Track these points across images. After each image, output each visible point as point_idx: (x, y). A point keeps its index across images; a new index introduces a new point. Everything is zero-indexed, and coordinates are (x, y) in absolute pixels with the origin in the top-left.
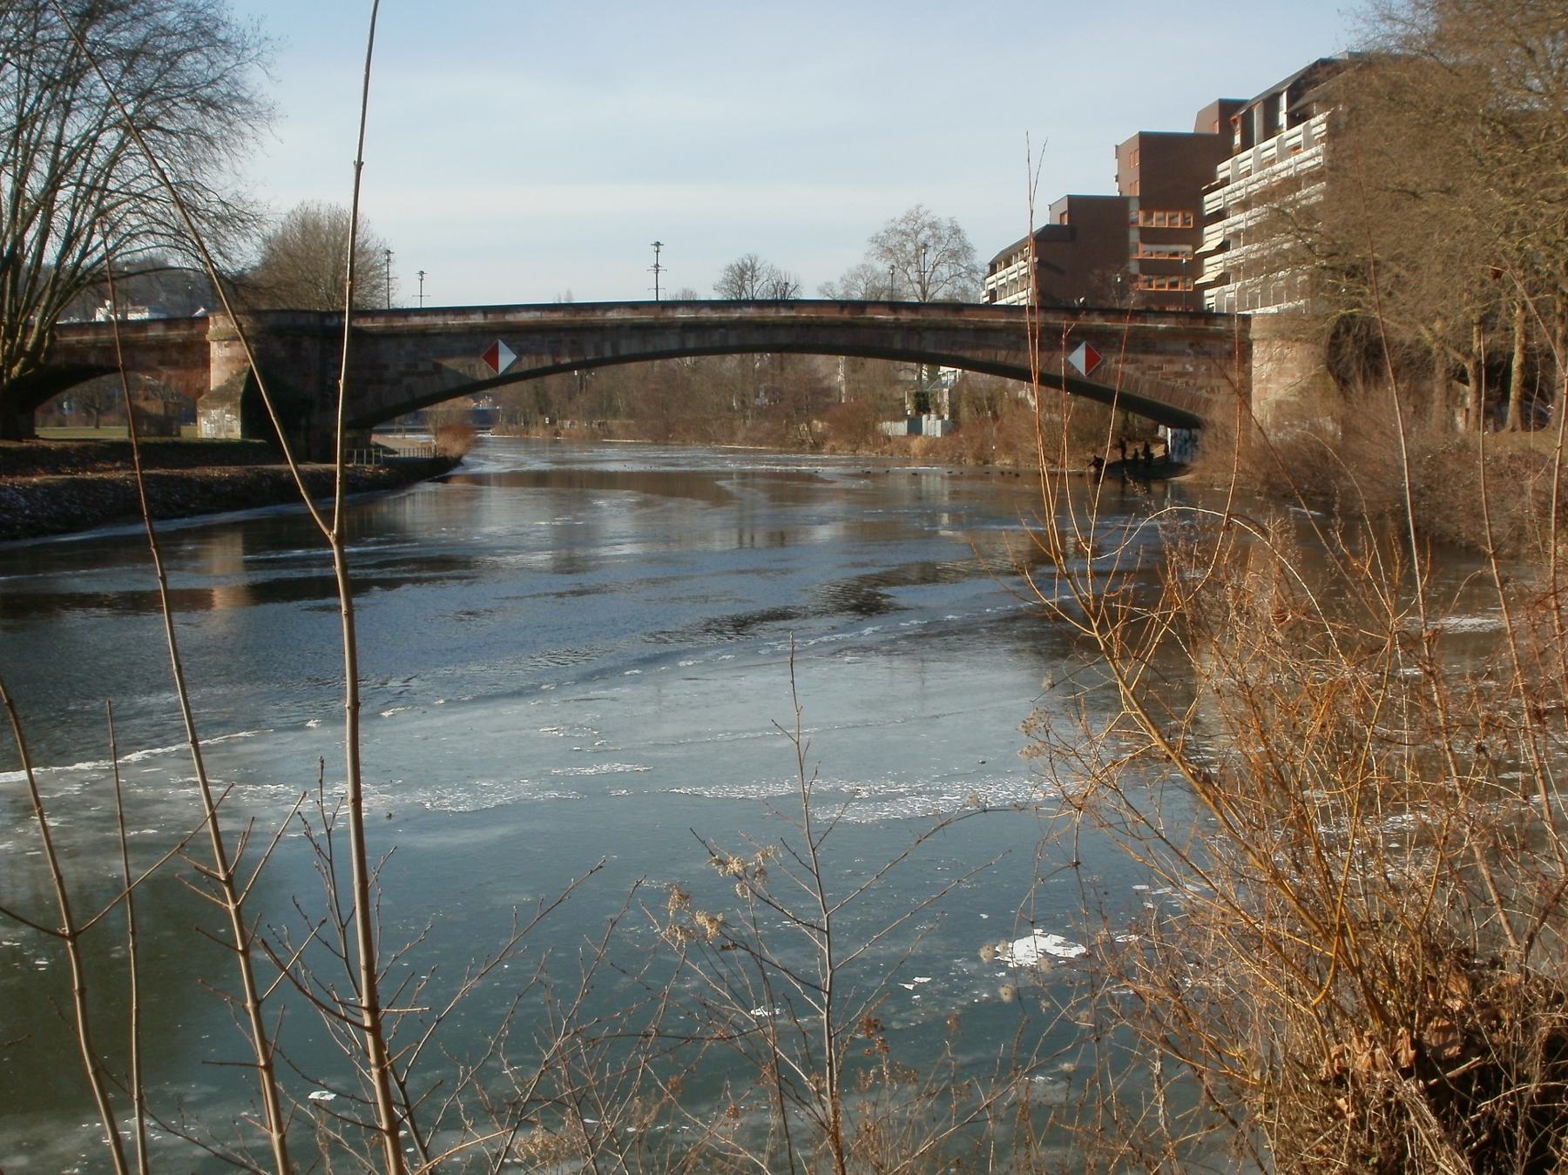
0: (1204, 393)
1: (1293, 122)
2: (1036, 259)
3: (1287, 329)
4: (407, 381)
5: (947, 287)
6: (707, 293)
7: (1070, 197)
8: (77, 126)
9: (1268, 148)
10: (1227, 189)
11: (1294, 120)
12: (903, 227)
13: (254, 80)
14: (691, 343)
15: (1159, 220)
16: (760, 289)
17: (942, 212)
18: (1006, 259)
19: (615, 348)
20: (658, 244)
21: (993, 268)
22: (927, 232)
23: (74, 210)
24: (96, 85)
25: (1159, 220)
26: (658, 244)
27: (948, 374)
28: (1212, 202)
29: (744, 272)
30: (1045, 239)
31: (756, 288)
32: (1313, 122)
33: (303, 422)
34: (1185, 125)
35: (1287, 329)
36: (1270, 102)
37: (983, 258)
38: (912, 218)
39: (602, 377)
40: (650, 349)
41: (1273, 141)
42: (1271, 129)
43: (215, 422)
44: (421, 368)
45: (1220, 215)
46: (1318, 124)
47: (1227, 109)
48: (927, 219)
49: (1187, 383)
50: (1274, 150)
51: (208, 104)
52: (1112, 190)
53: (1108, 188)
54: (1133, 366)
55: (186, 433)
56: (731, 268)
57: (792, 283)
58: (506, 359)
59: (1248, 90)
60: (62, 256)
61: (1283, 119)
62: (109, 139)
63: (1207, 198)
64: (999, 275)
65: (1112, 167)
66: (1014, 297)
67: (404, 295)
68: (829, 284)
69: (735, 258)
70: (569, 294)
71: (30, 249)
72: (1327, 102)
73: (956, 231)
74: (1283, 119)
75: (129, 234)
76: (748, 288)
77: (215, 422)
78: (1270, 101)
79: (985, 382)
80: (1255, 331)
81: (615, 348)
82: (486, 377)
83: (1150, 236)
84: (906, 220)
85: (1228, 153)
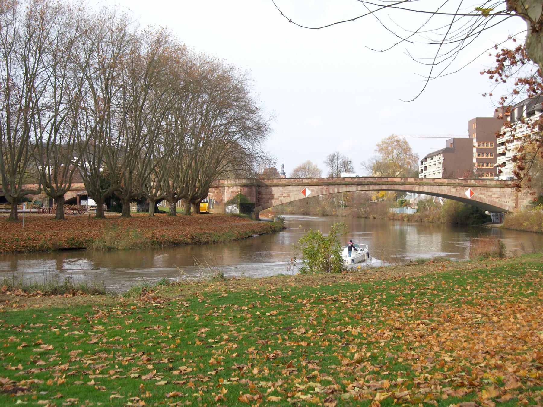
0: (504, 203)
4: (280, 198)
44: (284, 195)
48: (396, 139)
52: (466, 135)
56: (329, 156)
70: (273, 118)
84: (389, 139)
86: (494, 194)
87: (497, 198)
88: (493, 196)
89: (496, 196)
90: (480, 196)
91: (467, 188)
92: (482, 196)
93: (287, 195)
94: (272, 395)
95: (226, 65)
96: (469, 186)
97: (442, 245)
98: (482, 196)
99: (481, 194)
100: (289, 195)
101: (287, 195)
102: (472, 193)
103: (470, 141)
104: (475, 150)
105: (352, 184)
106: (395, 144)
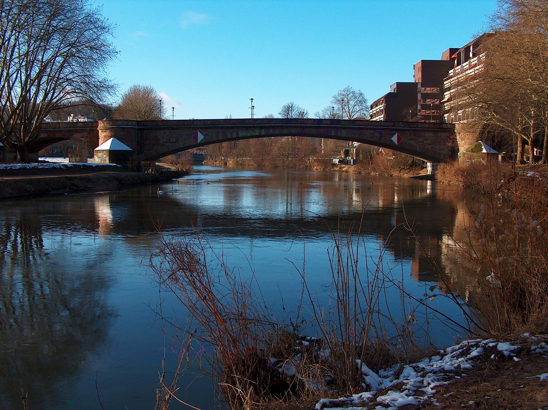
0: (438, 151)
1: (474, 56)
2: (385, 104)
3: (467, 128)
4: (166, 145)
5: (358, 114)
6: (277, 116)
7: (398, 84)
8: (48, 55)
9: (466, 65)
10: (452, 80)
11: (474, 56)
12: (343, 93)
13: (108, 38)
14: (263, 133)
15: (429, 90)
16: (294, 115)
17: (356, 88)
18: (376, 104)
19: (237, 134)
20: (252, 99)
21: (372, 108)
22: (351, 95)
23: (48, 84)
24: (55, 41)
25: (429, 90)
26: (252, 99)
27: (356, 144)
28: (447, 84)
29: (289, 108)
30: (388, 98)
31: (293, 114)
32: (481, 56)
33: (131, 158)
34: (438, 57)
35: (467, 128)
36: (467, 49)
37: (369, 103)
38: (347, 90)
39: (241, 143)
40: (249, 135)
41: (467, 63)
42: (467, 58)
43: (100, 158)
44: (172, 140)
45: (449, 89)
46: (482, 56)
47: (452, 51)
49: (432, 147)
50: (468, 66)
51: (92, 48)
52: (412, 80)
53: (410, 79)
54: (413, 141)
55: (90, 161)
56: (285, 107)
57: (305, 112)
58: (200, 137)
59: (460, 44)
60: (44, 99)
61: (471, 55)
62: (60, 59)
63: (445, 83)
64: (374, 110)
65: (412, 72)
66: (377, 118)
67: (168, 115)
68: (318, 112)
69: (286, 104)
70: (231, 116)
71: (33, 97)
72: (486, 49)
73: (361, 94)
74: (471, 55)
75: (67, 92)
76: (290, 114)
77: (100, 158)
78: (467, 49)
79: (366, 146)
80: (457, 127)
81: (237, 134)
82: (194, 144)
83: (425, 96)
85: (452, 67)
86: (427, 140)
87: (429, 144)
88: (425, 142)
89: (429, 142)
90: (409, 141)
91: (393, 132)
92: (412, 142)
93: (175, 140)
94: (169, 172)
95: (132, 85)
96: (397, 130)
97: (455, 220)
98: (412, 142)
99: (411, 139)
100: (177, 140)
101: (175, 140)
102: (399, 139)
103: (415, 84)
104: (419, 96)
105: (254, 127)
106: (351, 95)
